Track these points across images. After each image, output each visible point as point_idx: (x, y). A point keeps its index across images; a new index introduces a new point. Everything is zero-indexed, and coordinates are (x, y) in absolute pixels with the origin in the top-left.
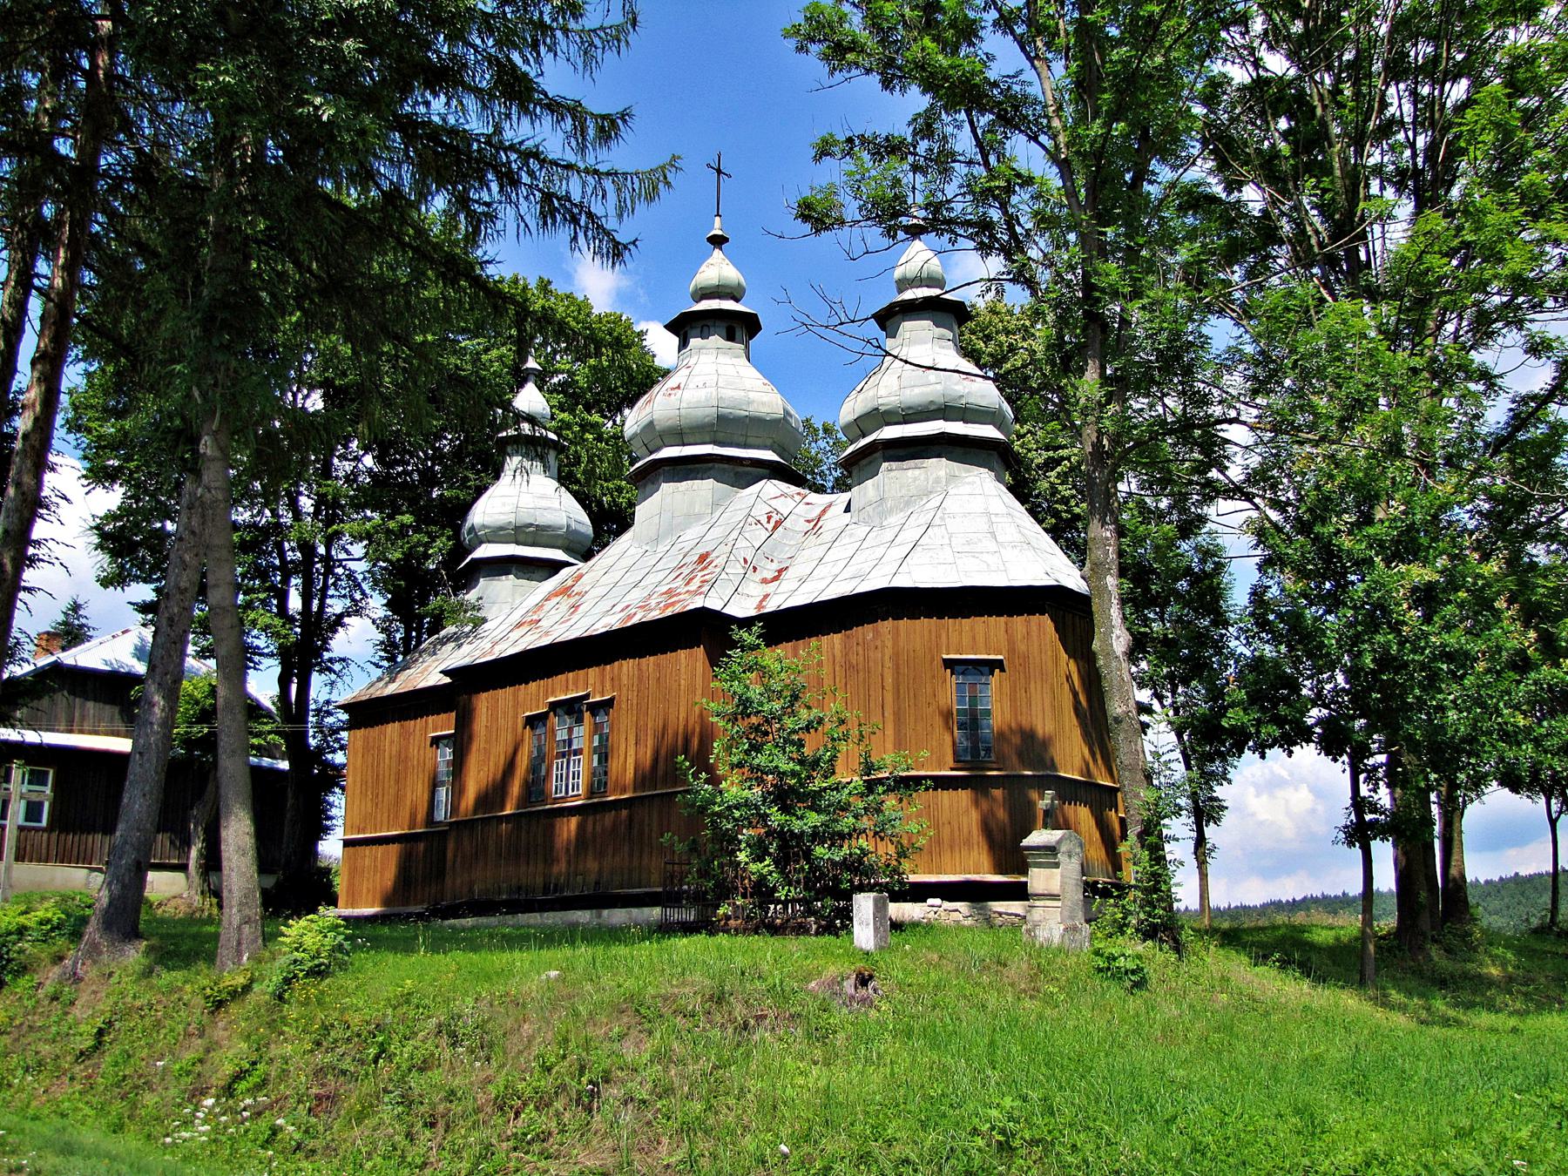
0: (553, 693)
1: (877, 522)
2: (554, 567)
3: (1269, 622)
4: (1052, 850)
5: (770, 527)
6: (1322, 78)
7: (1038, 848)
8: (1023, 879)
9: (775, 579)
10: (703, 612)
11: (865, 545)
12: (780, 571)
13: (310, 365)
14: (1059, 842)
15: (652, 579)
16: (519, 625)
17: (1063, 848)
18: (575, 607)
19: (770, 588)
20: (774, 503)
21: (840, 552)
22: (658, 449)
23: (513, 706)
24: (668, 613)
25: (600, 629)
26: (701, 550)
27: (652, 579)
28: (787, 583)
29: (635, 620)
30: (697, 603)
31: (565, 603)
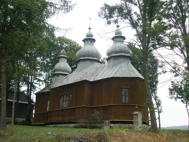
0: (64, 92)
1: (111, 68)
2: (66, 75)
3: (148, 40)
4: (137, 115)
5: (96, 69)
6: (168, 35)
7: (135, 114)
8: (133, 121)
9: (97, 76)
10: (85, 80)
11: (110, 71)
12: (97, 75)
13: (23, 16)
14: (138, 114)
15: (79, 76)
16: (60, 82)
17: (139, 115)
18: (68, 80)
19: (95, 77)
20: (97, 66)
21: (106, 72)
22: (80, 58)
23: (64, 122)
24: (81, 80)
25: (71, 83)
26: (86, 72)
27: (79, 76)
28: (98, 77)
29: (76, 82)
30: (85, 79)
31: (67, 79)
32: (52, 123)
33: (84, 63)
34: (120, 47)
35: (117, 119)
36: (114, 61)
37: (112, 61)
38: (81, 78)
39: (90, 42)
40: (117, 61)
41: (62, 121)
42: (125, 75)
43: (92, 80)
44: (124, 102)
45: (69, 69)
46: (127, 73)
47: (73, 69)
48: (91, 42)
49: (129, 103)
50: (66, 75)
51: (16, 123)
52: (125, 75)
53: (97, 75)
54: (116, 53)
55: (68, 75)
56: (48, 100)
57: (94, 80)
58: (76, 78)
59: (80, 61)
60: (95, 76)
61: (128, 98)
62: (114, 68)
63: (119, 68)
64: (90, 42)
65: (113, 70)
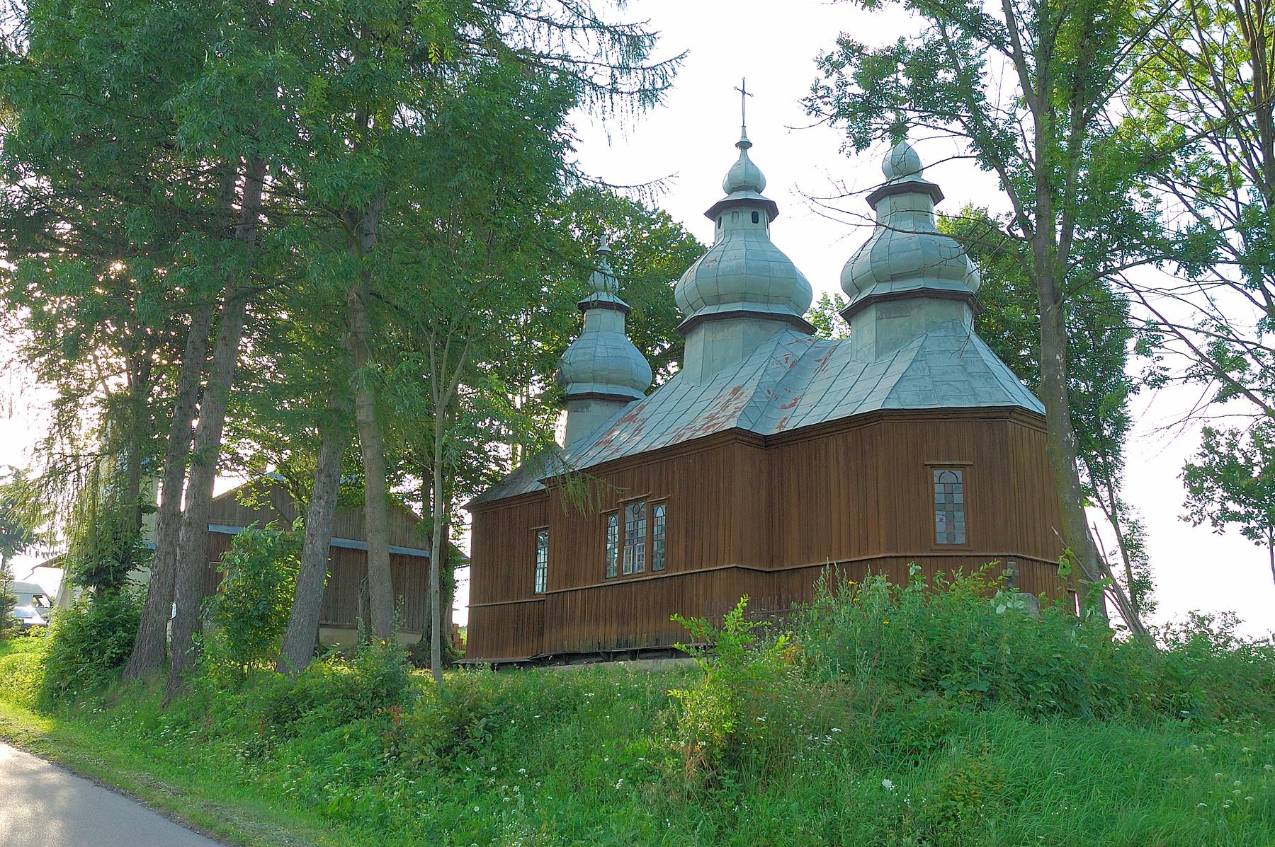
5: (788, 365)
12: (796, 400)
28: (799, 411)
33: (720, 335)
36: (884, 321)
40: (902, 320)
41: (618, 645)
50: (624, 400)
54: (894, 278)
57: (780, 426)
60: (784, 407)
62: (886, 359)
63: (914, 361)
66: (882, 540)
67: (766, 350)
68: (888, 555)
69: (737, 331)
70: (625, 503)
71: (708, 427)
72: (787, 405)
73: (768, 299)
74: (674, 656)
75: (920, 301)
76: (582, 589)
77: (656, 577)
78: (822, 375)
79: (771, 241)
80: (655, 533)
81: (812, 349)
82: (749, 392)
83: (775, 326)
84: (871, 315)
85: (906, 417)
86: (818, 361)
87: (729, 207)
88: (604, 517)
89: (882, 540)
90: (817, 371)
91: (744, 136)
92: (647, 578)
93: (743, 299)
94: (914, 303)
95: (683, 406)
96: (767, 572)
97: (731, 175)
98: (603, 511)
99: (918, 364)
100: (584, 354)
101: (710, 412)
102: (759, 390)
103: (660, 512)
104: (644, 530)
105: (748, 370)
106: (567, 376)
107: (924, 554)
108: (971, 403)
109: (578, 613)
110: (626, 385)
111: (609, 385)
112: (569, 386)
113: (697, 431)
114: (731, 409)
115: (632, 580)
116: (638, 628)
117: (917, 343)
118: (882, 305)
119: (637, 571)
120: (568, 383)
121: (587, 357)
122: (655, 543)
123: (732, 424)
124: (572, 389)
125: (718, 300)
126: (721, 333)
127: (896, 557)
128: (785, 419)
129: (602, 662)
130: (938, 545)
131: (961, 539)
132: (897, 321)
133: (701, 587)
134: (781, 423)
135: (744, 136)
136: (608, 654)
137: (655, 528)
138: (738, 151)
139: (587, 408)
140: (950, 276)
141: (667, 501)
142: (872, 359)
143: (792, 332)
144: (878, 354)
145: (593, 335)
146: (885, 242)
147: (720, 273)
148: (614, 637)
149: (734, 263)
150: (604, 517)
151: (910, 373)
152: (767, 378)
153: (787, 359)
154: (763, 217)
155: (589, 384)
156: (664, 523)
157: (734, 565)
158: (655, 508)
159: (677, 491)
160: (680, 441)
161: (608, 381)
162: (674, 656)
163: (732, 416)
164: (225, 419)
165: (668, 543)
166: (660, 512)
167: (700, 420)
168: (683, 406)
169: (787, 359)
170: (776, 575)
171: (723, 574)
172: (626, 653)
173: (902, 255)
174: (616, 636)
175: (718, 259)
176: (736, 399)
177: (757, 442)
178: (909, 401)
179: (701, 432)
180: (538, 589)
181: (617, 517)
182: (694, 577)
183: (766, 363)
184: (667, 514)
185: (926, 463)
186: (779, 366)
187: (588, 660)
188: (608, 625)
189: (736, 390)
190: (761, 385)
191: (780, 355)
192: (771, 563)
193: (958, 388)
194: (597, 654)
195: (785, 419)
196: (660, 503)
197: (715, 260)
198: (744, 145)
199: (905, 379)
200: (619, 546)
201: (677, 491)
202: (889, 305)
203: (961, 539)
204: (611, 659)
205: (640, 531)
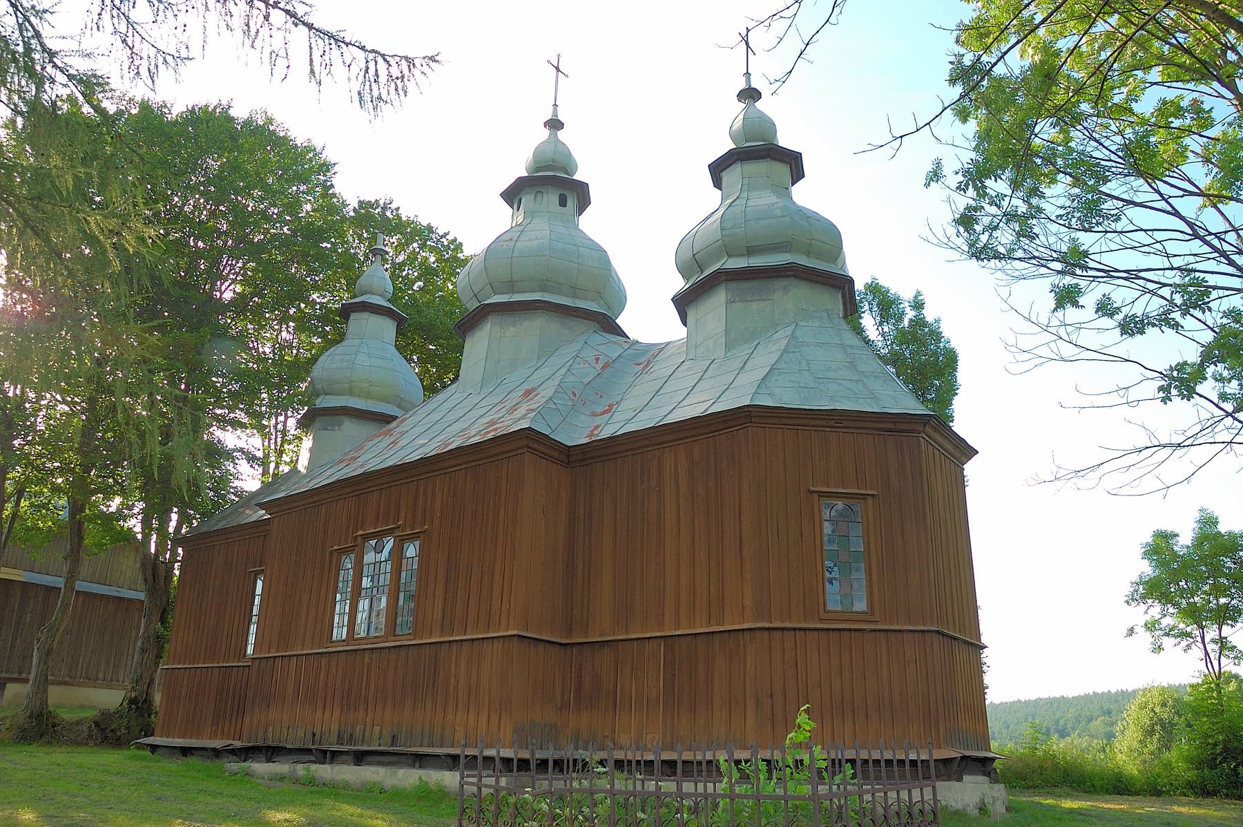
5: (599, 366)
12: (611, 406)
16: (341, 461)
24: (490, 436)
28: (617, 417)
32: (268, 747)
33: (511, 331)
34: (778, 213)
35: (1191, 816)
36: (738, 305)
37: (716, 305)
38: (493, 423)
39: (552, 198)
40: (762, 304)
41: (340, 741)
42: (832, 398)
43: (574, 436)
44: (839, 608)
45: (407, 375)
46: (849, 384)
47: (431, 390)
48: (563, 202)
49: (872, 614)
50: (387, 419)
51: (956, 381)
52: (832, 398)
53: (611, 406)
54: (751, 251)
55: (395, 418)
56: (256, 574)
57: (591, 435)
58: (457, 427)
59: (483, 313)
60: (595, 415)
61: (246, 651)
62: (742, 352)
63: (785, 351)
64: (552, 198)
65: (738, 364)
66: (748, 602)
67: (570, 350)
68: (758, 625)
69: (533, 329)
70: (367, 538)
71: (489, 432)
72: (598, 411)
73: (574, 292)
74: (417, 764)
75: (785, 282)
76: (298, 655)
77: (398, 643)
78: (645, 377)
79: (580, 227)
80: (403, 581)
81: (628, 352)
82: (547, 392)
83: (579, 326)
84: (719, 299)
85: (784, 421)
86: (637, 364)
87: (533, 186)
88: (335, 554)
89: (748, 602)
90: (637, 375)
91: (555, 113)
92: (387, 645)
93: (544, 289)
94: (779, 283)
95: (453, 416)
96: (561, 644)
97: (537, 153)
98: (336, 547)
99: (791, 355)
100: (342, 361)
101: (492, 417)
102: (561, 390)
103: (411, 551)
104: (388, 575)
105: (545, 371)
106: (319, 386)
107: (811, 626)
108: (873, 407)
109: (290, 690)
110: (389, 403)
111: (369, 401)
112: (320, 399)
113: (472, 437)
114: (522, 411)
115: (365, 647)
116: (369, 718)
117: (784, 334)
118: (733, 285)
119: (372, 634)
120: (318, 395)
121: (345, 364)
122: (402, 595)
123: (524, 424)
124: (322, 402)
125: (511, 287)
126: (511, 329)
127: (769, 629)
128: (597, 427)
129: (315, 762)
130: (829, 612)
131: (861, 606)
132: (755, 305)
133: (463, 663)
134: (592, 431)
135: (555, 113)
136: (325, 752)
137: (403, 574)
138: (545, 133)
139: (339, 425)
140: (820, 256)
141: (422, 535)
142: (720, 352)
143: (602, 334)
144: (728, 347)
145: (356, 342)
146: (738, 209)
147: (516, 254)
148: (335, 727)
149: (536, 242)
150: (335, 554)
151: (781, 365)
152: (570, 378)
153: (597, 359)
154: (572, 202)
155: (344, 397)
156: (415, 567)
157: (515, 632)
158: (406, 545)
159: (437, 523)
160: (446, 450)
161: (369, 396)
162: (417, 764)
163: (524, 417)
164: (196, 525)
165: (419, 597)
166: (411, 551)
167: (477, 426)
168: (453, 416)
169: (597, 359)
170: (575, 649)
171: (498, 645)
172: (347, 753)
173: (762, 222)
174: (337, 727)
175: (515, 239)
176: (528, 401)
177: (556, 455)
178: (784, 396)
179: (478, 437)
180: (250, 650)
181: (353, 556)
182: (454, 647)
183: (569, 363)
184: (422, 554)
185: (812, 489)
186: (587, 365)
187: (295, 758)
188: (327, 712)
189: (528, 393)
190: (562, 385)
191: (589, 355)
192: (569, 631)
193: (850, 389)
194: (309, 751)
195: (597, 427)
196: (411, 538)
197: (511, 240)
198: (555, 124)
199: (776, 372)
200: (352, 596)
201: (437, 523)
202: (745, 285)
203: (861, 606)
204: (328, 760)
205: (382, 577)
